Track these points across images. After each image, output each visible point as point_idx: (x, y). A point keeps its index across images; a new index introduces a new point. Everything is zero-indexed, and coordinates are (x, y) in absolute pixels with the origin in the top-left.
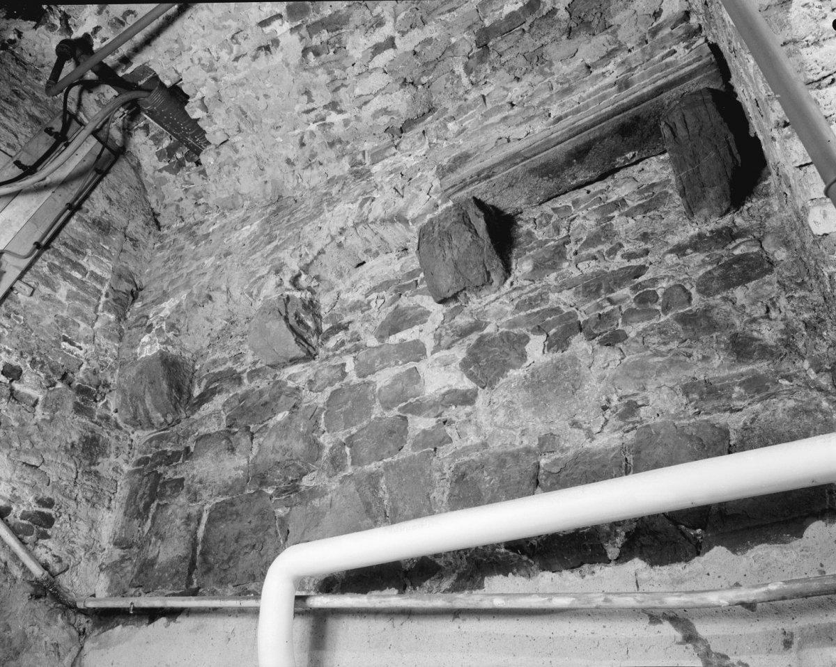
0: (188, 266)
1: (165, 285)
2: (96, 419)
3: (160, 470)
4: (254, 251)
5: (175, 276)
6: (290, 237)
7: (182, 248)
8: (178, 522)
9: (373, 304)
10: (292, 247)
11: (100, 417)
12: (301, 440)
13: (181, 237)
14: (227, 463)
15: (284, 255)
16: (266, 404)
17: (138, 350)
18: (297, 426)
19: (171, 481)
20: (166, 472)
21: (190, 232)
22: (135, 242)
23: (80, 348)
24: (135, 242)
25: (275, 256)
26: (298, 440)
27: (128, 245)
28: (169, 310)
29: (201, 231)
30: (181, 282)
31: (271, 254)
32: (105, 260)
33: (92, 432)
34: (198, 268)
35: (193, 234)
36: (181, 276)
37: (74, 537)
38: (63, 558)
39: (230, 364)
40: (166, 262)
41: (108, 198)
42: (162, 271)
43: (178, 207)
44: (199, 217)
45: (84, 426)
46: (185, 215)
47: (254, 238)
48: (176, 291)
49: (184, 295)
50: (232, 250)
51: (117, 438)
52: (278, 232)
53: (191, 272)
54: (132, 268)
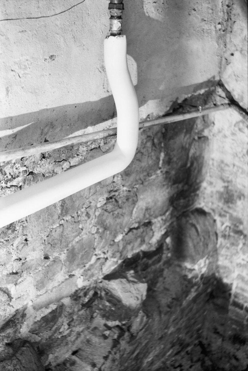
0: (182, 323)
1: (195, 307)
2: (228, 215)
3: (186, 187)
4: (146, 344)
5: (190, 315)
6: (125, 363)
7: (187, 333)
8: (175, 159)
9: (66, 327)
10: (125, 356)
11: (225, 216)
12: (108, 225)
13: (188, 340)
14: (150, 200)
15: (129, 349)
16: (129, 244)
17: (207, 262)
18: (111, 233)
19: (180, 183)
20: (183, 187)
21: (183, 345)
22: (216, 332)
23: (243, 260)
24: (216, 332)
25: (135, 346)
26: (110, 224)
27: (220, 329)
28: (192, 292)
29: (177, 348)
30: (186, 311)
31: (136, 347)
32: (234, 317)
33: (229, 207)
34: (177, 323)
35: (181, 344)
36: (186, 315)
37: (233, 144)
38: (238, 131)
39: (150, 262)
40: (195, 322)
41: (237, 359)
42: (197, 315)
43: (192, 360)
44: (178, 357)
45: (235, 211)
46: (187, 357)
47: (145, 356)
48: (189, 305)
49: (184, 303)
50: (158, 342)
51: (213, 203)
52: (133, 363)
53: (181, 319)
54: (216, 314)
